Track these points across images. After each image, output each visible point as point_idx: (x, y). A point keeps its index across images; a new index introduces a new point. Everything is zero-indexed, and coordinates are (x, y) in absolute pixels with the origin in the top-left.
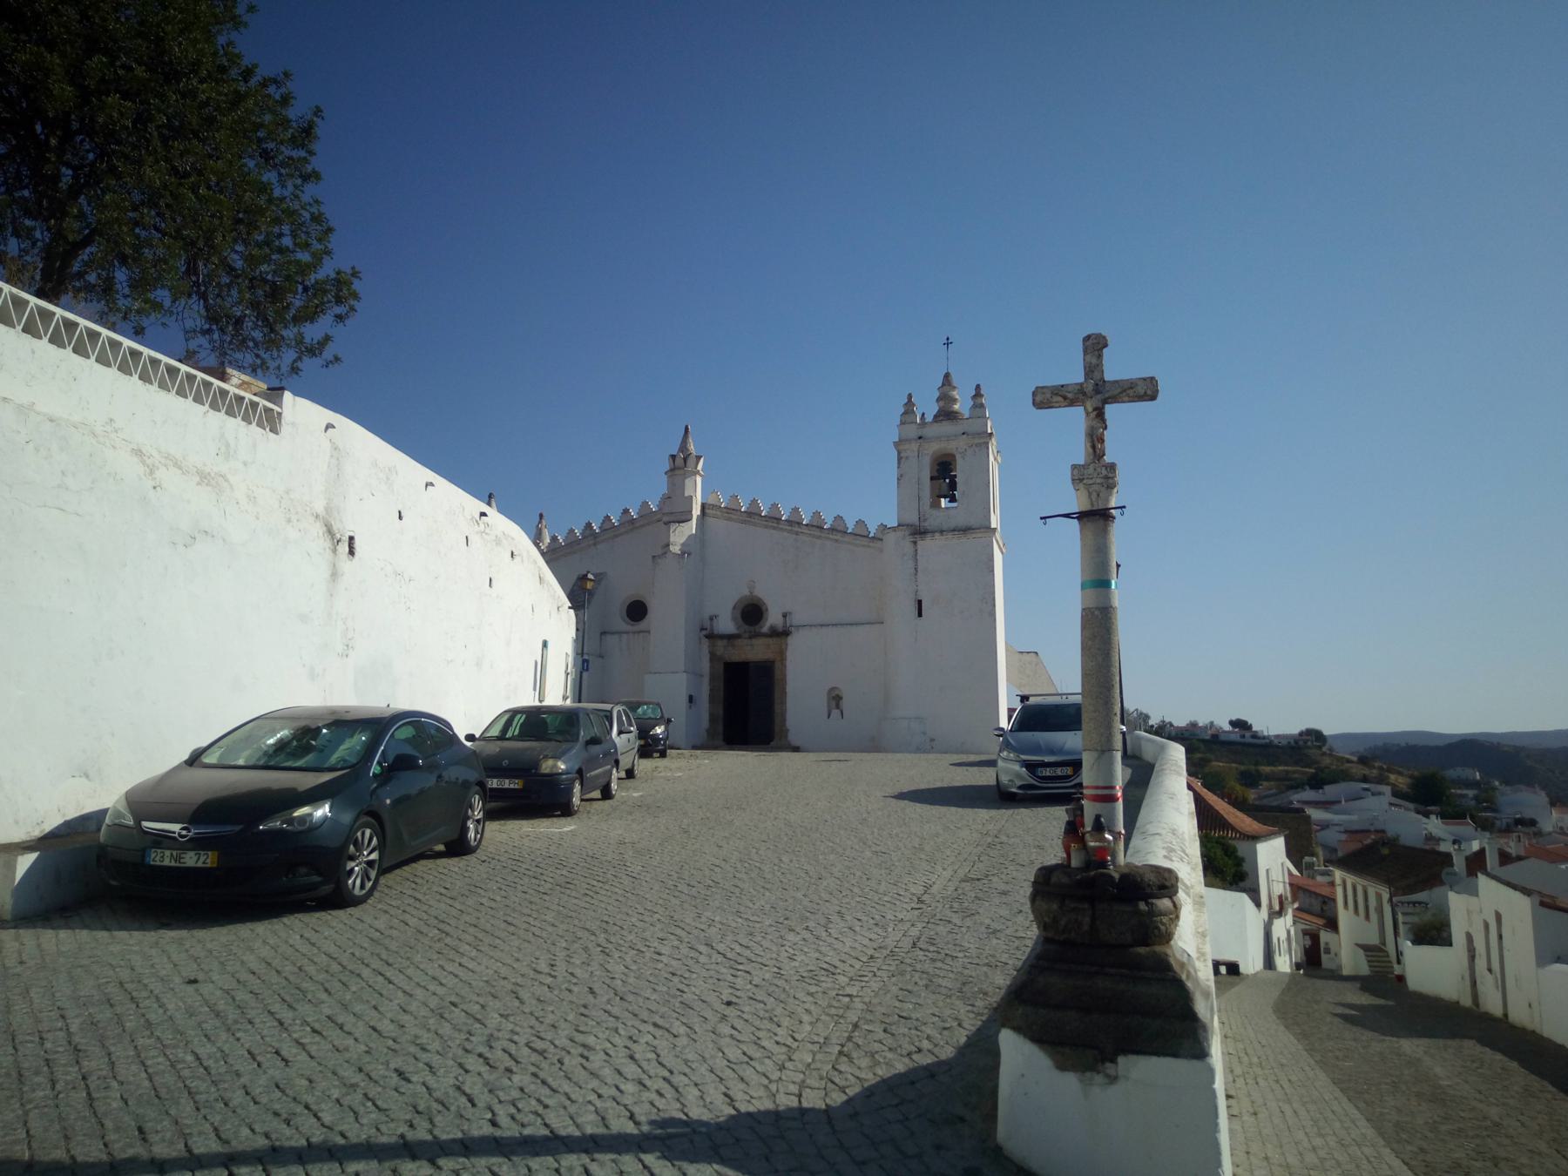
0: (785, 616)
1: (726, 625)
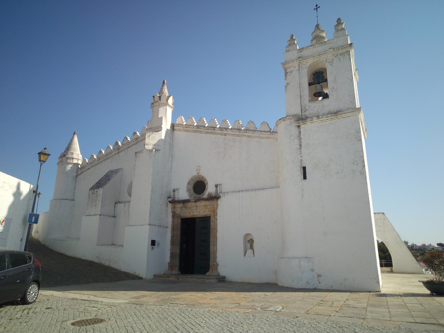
0: (216, 186)
1: (183, 194)
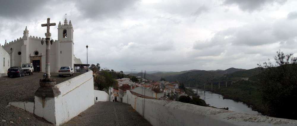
1: (33, 55)
